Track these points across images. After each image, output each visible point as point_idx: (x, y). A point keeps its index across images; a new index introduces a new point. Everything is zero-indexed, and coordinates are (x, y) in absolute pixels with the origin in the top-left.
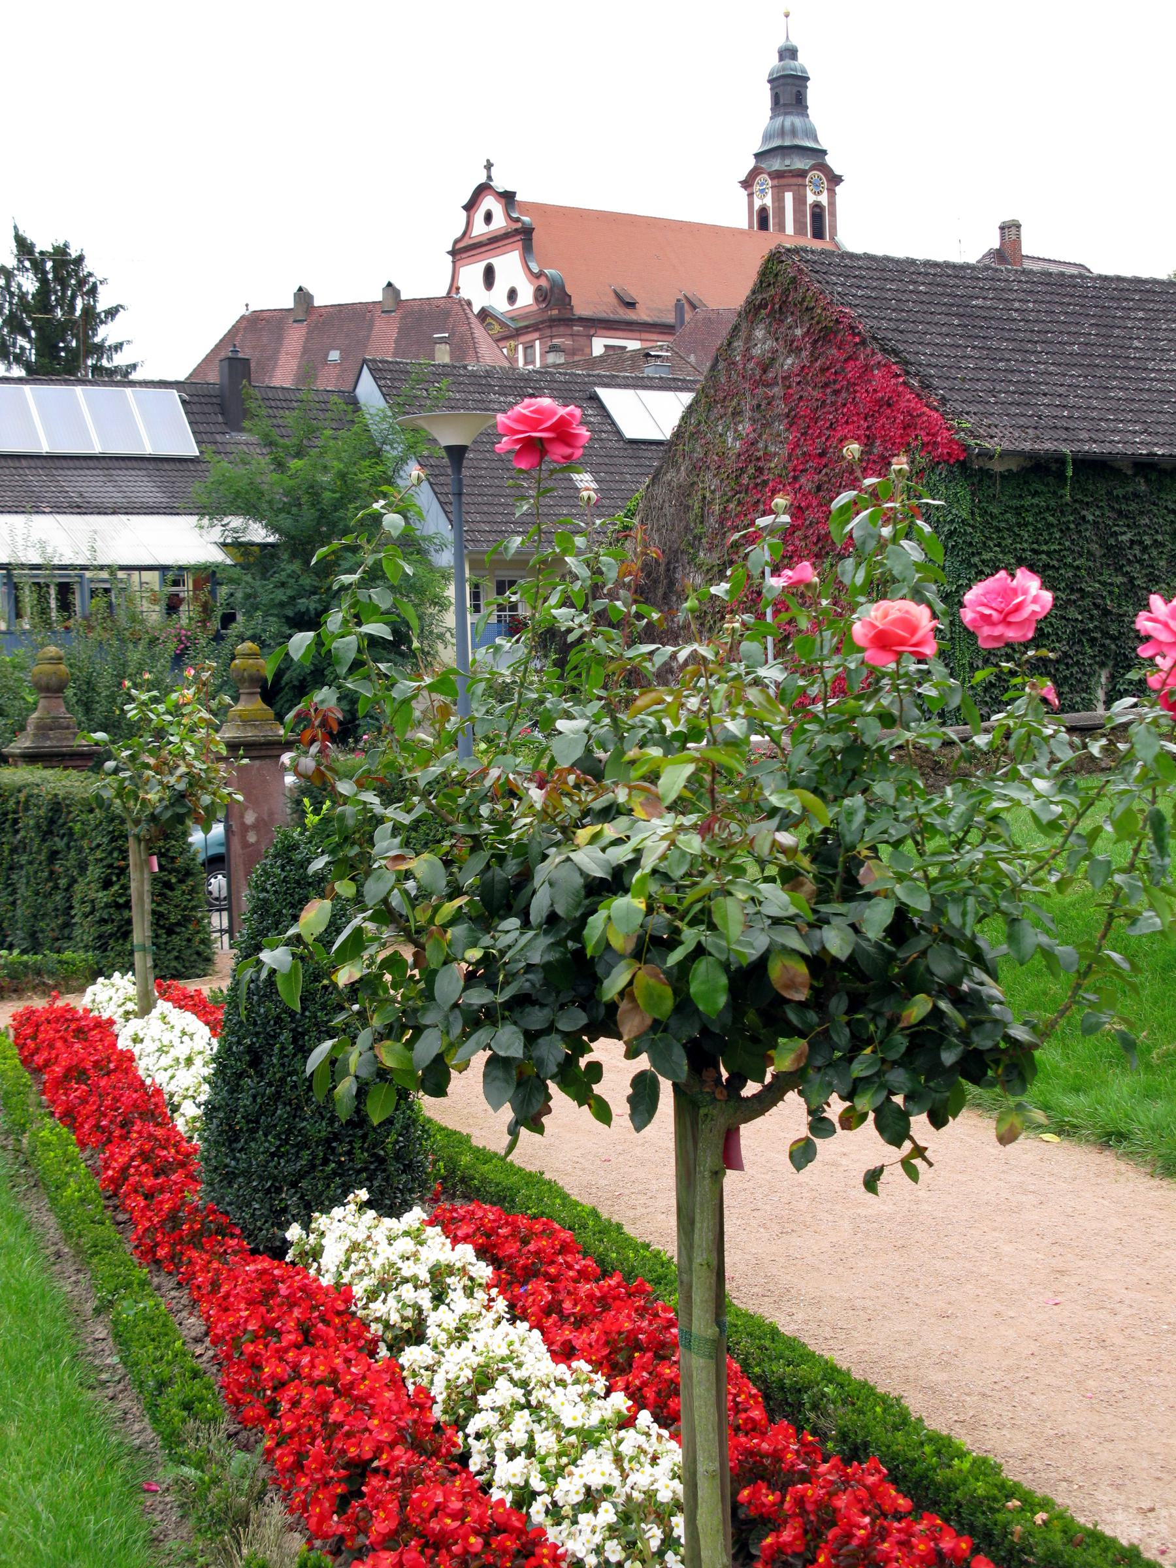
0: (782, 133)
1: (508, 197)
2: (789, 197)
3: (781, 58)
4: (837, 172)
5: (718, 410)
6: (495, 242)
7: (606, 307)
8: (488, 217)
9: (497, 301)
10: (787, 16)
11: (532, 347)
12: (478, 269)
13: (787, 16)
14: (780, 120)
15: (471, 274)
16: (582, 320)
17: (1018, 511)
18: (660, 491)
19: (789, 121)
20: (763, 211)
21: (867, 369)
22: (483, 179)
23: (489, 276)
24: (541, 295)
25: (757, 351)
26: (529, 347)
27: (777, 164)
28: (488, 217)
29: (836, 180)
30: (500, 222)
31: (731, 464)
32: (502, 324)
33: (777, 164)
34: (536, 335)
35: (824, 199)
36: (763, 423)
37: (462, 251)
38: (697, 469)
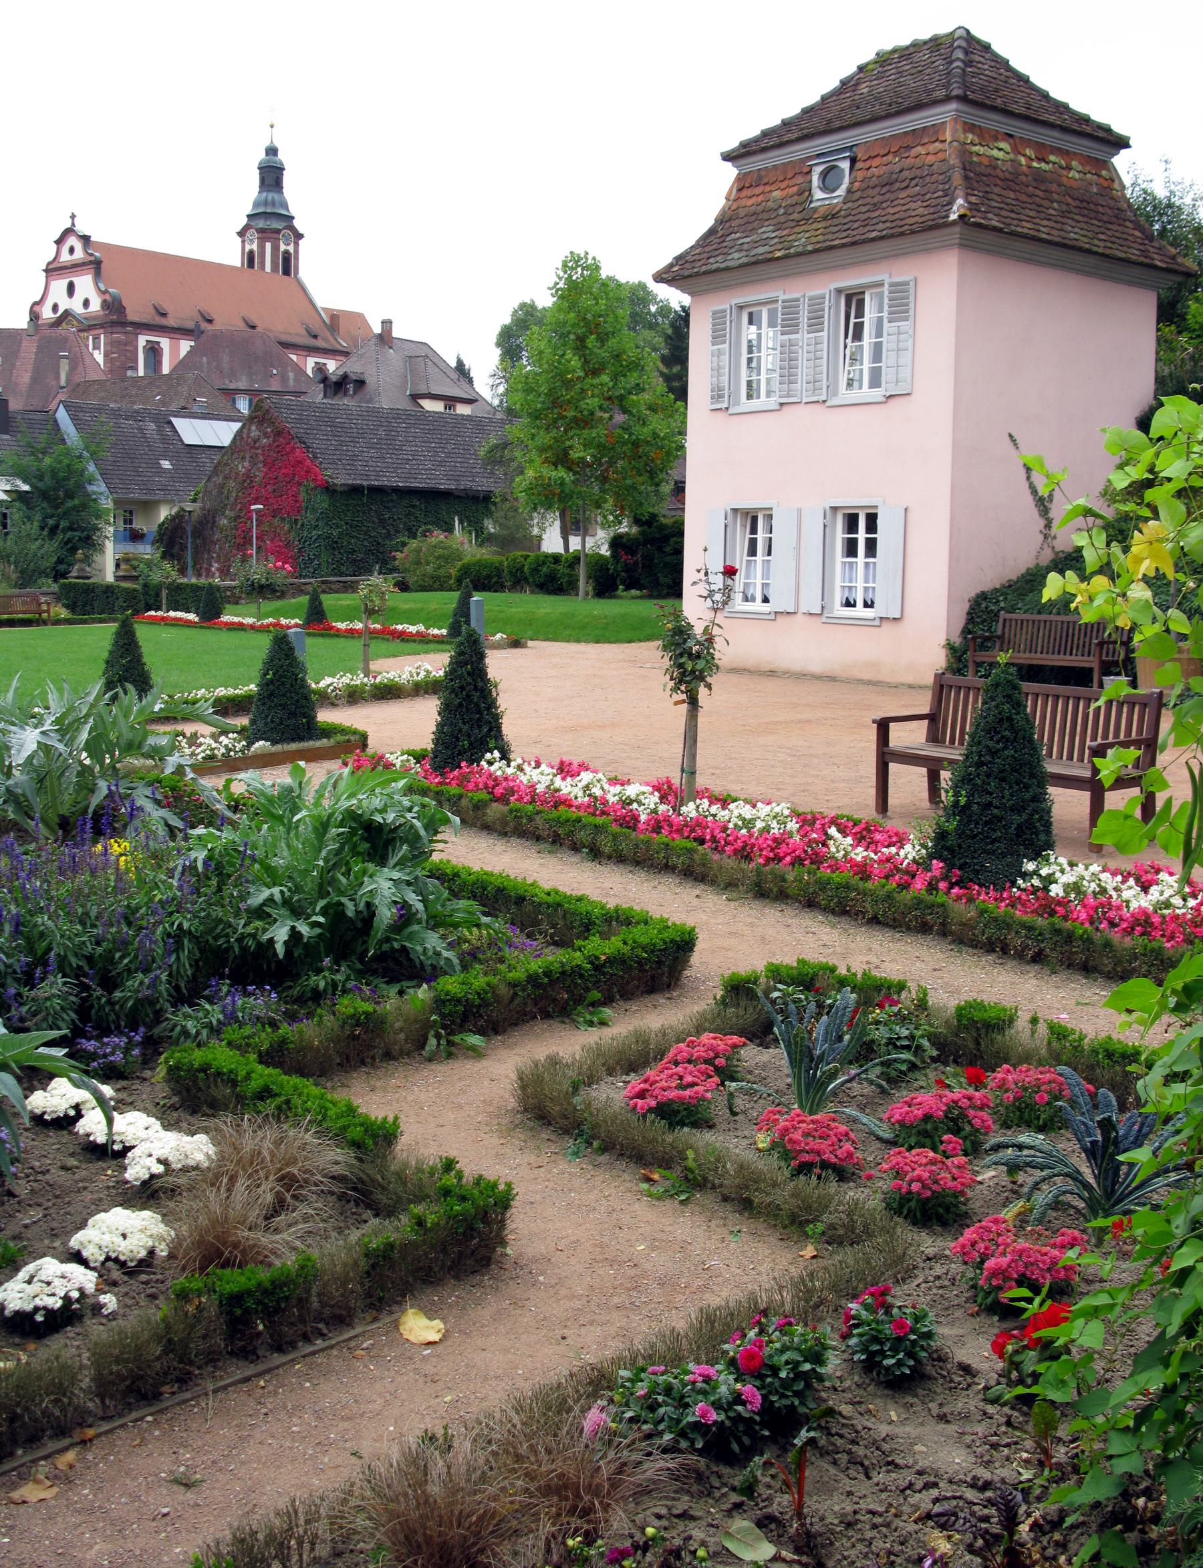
0: (266, 203)
1: (86, 239)
2: (268, 246)
3: (267, 154)
4: (301, 231)
5: (236, 455)
6: (76, 267)
7: (147, 316)
8: (72, 250)
9: (76, 306)
10: (272, 126)
11: (99, 338)
12: (64, 283)
13: (272, 126)
14: (265, 194)
15: (59, 286)
16: (133, 324)
17: (347, 505)
18: (211, 485)
19: (271, 196)
20: (251, 253)
21: (294, 448)
22: (69, 225)
23: (71, 289)
24: (105, 305)
25: (252, 435)
26: (96, 338)
27: (261, 224)
28: (72, 250)
29: (299, 236)
30: (79, 254)
31: (241, 479)
32: (79, 321)
33: (261, 224)
34: (102, 331)
35: (291, 248)
36: (253, 462)
37: (53, 270)
38: (226, 478)
